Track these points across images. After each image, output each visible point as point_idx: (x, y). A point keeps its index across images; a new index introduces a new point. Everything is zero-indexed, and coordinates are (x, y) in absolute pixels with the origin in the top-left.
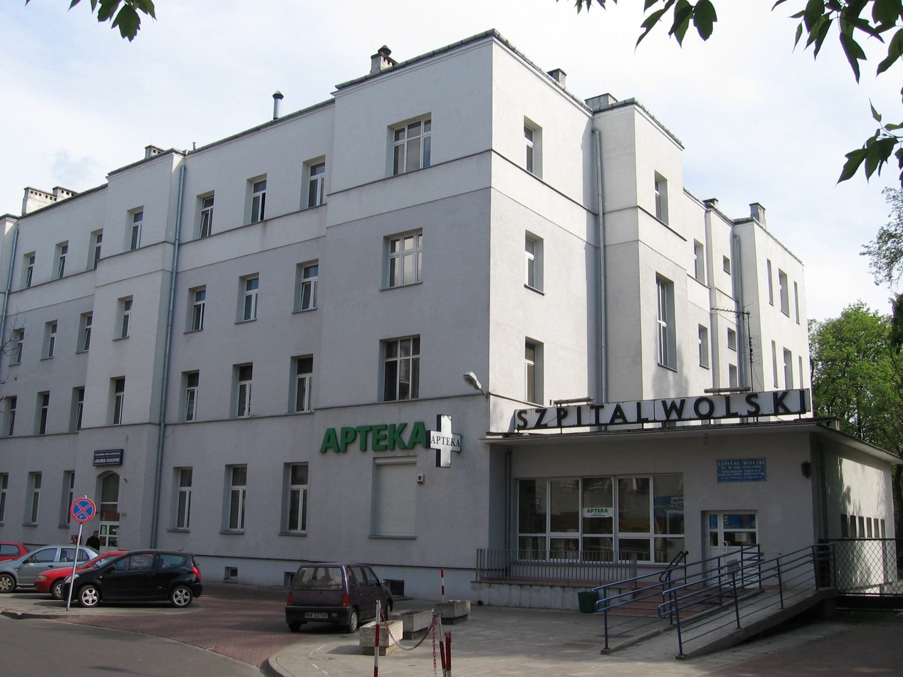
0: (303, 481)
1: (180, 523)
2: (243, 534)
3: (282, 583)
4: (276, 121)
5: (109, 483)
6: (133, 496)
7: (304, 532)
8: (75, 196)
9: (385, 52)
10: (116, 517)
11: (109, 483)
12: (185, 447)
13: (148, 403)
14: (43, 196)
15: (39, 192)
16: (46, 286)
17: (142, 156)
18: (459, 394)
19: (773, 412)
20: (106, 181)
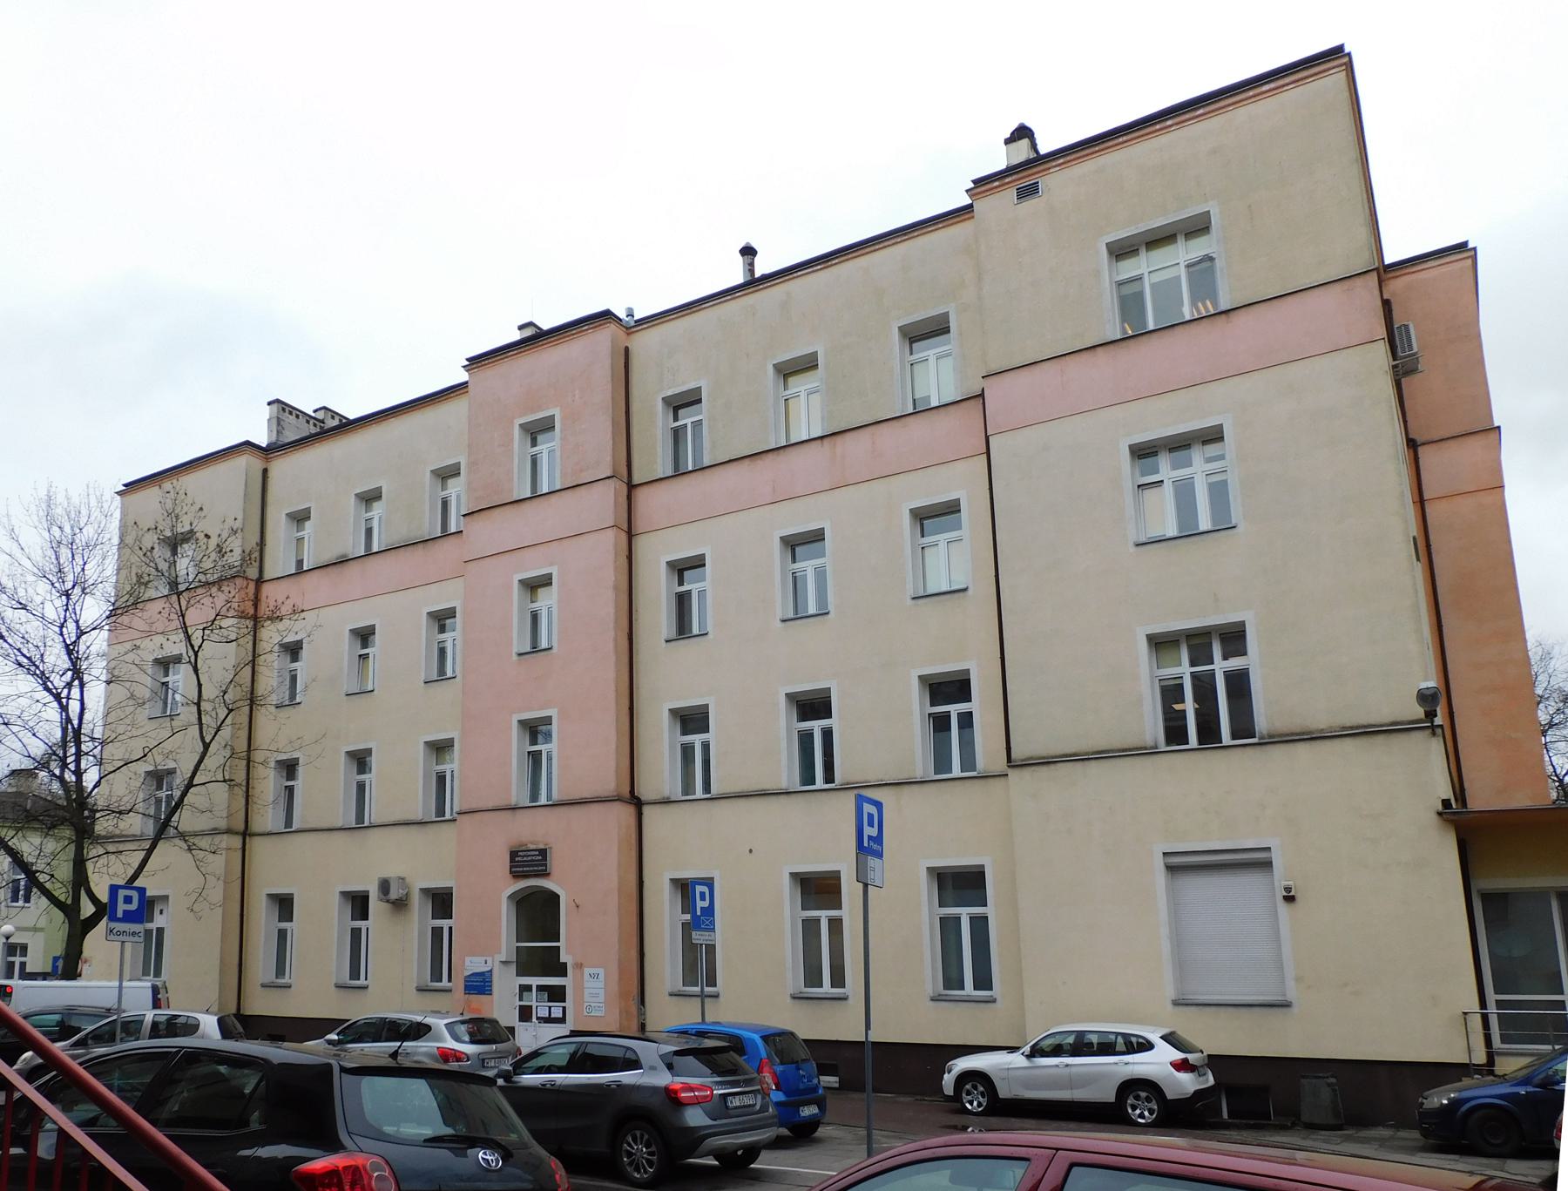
0: (448, 915)
1: (355, 974)
2: (366, 987)
3: (1113, 1100)
4: (753, 283)
5: (538, 914)
6: (586, 937)
7: (837, 991)
8: (347, 426)
9: (1022, 133)
10: (561, 970)
11: (538, 914)
12: (682, 842)
13: (613, 764)
14: (302, 419)
15: (298, 413)
16: (747, 461)
17: (516, 336)
18: (1328, 743)
19: (1482, 799)
20: (463, 376)
